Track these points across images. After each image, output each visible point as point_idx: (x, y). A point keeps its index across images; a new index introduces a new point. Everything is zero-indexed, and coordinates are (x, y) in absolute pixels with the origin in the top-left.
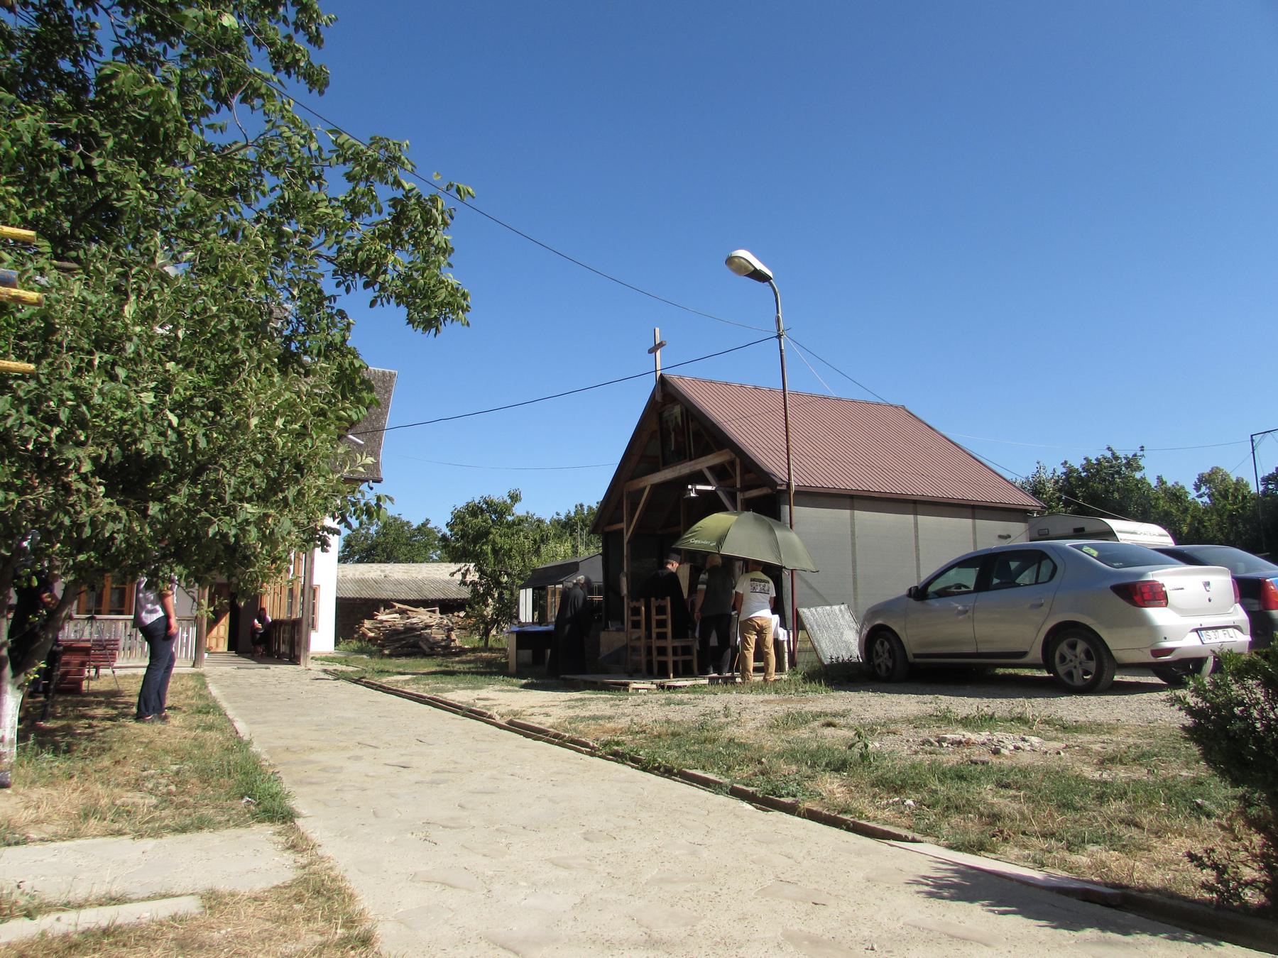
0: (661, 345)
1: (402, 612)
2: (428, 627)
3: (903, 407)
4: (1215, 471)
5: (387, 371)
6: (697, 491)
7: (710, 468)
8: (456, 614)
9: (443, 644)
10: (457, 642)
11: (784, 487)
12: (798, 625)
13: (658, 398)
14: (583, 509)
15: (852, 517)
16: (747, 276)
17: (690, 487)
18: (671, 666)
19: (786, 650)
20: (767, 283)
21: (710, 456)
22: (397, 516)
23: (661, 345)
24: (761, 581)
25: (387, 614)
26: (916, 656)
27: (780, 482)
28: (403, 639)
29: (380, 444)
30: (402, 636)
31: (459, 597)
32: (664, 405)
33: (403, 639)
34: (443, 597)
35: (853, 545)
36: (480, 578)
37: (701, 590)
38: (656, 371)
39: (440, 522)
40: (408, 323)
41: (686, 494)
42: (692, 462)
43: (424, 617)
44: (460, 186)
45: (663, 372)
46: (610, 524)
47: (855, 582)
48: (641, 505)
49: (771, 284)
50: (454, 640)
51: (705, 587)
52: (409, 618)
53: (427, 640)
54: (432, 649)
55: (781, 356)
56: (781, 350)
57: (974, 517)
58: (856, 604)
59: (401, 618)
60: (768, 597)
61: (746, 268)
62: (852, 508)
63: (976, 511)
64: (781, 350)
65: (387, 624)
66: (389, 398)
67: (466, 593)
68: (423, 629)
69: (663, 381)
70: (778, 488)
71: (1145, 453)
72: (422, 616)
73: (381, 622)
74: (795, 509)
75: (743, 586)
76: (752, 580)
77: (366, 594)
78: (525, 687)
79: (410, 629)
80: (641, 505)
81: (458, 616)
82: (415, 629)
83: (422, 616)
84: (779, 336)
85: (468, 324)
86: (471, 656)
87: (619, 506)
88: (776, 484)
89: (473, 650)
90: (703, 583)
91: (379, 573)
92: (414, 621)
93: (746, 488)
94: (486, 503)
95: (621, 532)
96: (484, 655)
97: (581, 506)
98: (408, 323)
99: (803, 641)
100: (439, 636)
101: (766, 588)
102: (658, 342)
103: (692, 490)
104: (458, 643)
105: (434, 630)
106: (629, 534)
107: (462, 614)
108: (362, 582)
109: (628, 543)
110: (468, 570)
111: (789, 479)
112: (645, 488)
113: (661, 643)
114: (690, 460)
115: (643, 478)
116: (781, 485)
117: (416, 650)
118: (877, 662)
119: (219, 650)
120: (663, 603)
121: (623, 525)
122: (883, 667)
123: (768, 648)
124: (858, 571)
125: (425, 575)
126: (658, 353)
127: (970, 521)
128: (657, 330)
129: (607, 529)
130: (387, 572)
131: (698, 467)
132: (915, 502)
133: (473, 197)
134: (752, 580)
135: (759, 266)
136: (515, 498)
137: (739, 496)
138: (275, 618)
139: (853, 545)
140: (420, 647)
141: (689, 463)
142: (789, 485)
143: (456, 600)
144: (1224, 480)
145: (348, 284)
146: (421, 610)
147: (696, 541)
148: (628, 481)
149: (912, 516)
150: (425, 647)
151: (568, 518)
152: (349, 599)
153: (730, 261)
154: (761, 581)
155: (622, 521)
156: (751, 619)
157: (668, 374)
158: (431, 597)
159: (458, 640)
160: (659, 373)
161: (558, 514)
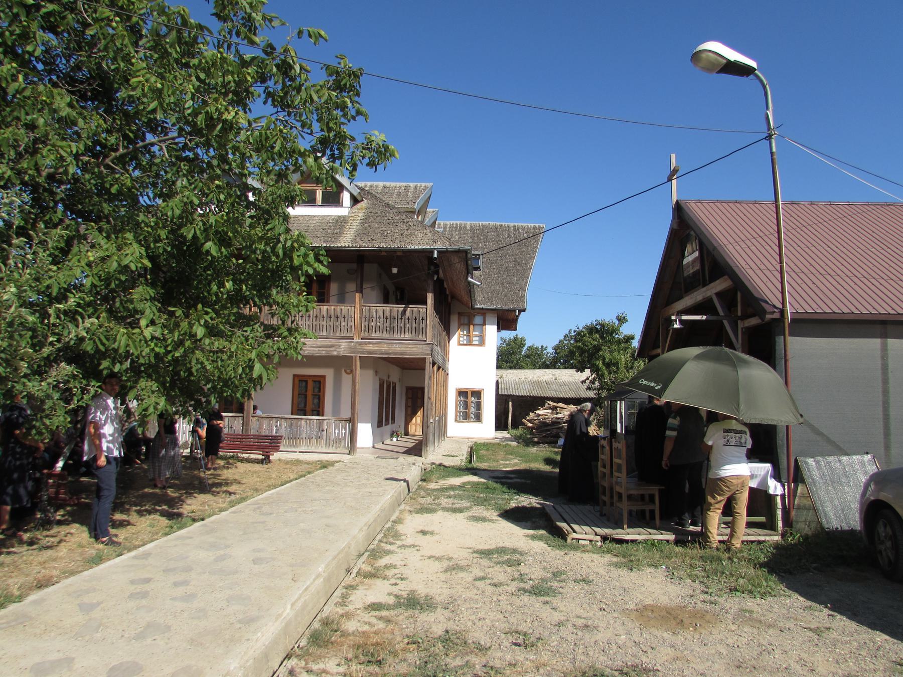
1: (554, 408)
5: (541, 225)
11: (777, 316)
12: (797, 477)
15: (884, 349)
16: (719, 72)
19: (779, 505)
20: (752, 77)
21: (718, 282)
24: (736, 432)
28: (549, 430)
29: (526, 282)
30: (549, 428)
33: (549, 430)
35: (885, 381)
37: (670, 437)
42: (705, 289)
44: (309, 29)
51: (674, 433)
52: (557, 413)
55: (773, 160)
60: (745, 449)
62: (884, 336)
64: (772, 154)
65: (540, 418)
73: (539, 415)
74: (790, 339)
75: (713, 437)
76: (727, 431)
77: (535, 393)
82: (559, 423)
84: (769, 137)
88: (765, 312)
90: (672, 429)
91: (551, 376)
92: (559, 416)
103: (676, 320)
108: (538, 383)
111: (783, 303)
114: (704, 286)
119: (417, 434)
124: (892, 412)
130: (557, 376)
131: (709, 294)
133: (326, 40)
135: (733, 56)
139: (885, 381)
142: (782, 312)
152: (522, 396)
153: (696, 57)
154: (736, 432)
155: (659, 347)
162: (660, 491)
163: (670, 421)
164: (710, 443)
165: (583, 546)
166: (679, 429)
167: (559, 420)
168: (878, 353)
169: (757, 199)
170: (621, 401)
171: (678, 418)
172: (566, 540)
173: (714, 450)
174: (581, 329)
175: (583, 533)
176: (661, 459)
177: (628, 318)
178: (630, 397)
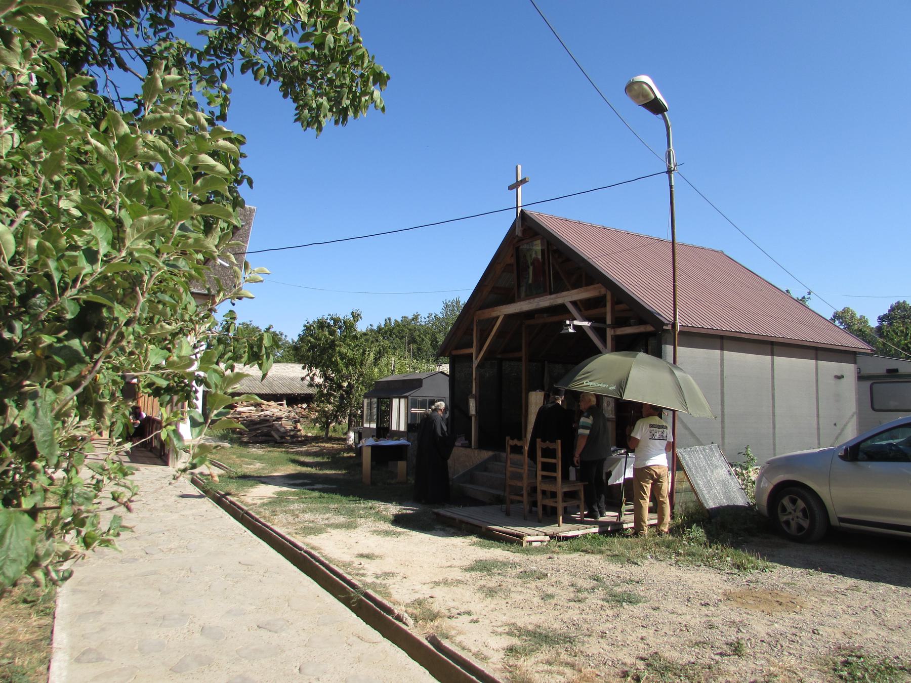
0: (524, 181)
1: (257, 405)
2: (279, 419)
3: (722, 252)
4: (846, 310)
5: (252, 207)
6: (575, 327)
7: (574, 303)
8: (300, 405)
9: (292, 433)
10: (302, 432)
11: (669, 327)
13: (519, 232)
14: (390, 322)
17: (568, 322)
18: (560, 511)
20: (660, 116)
22: (249, 323)
23: (524, 181)
25: (245, 406)
26: (842, 520)
27: (666, 322)
28: (258, 429)
30: (258, 426)
31: (302, 392)
32: (521, 240)
33: (258, 429)
34: (289, 392)
36: (325, 381)
37: (583, 435)
38: (517, 207)
39: (292, 333)
40: (296, 121)
41: (562, 329)
42: (553, 296)
43: (275, 410)
45: (523, 208)
46: (456, 348)
47: (723, 422)
48: (493, 333)
49: (665, 118)
50: (300, 430)
51: (587, 432)
52: (262, 411)
53: (278, 430)
54: (282, 437)
55: (671, 192)
56: (671, 187)
57: (817, 359)
58: (723, 444)
59: (257, 410)
60: (665, 442)
61: (646, 95)
63: (725, 342)
64: (671, 187)
65: (244, 415)
66: (249, 229)
67: (313, 391)
68: (274, 421)
69: (523, 217)
70: (664, 327)
71: (812, 296)
72: (273, 409)
73: (240, 413)
76: (652, 426)
78: (399, 521)
79: (265, 421)
80: (493, 333)
81: (301, 408)
82: (268, 421)
83: (273, 409)
84: (669, 172)
85: (383, 109)
86: (314, 447)
87: (469, 332)
88: (664, 324)
89: (316, 439)
90: (585, 427)
93: (619, 322)
94: (332, 318)
95: (471, 355)
96: (327, 445)
97: (389, 319)
98: (296, 121)
99: (680, 481)
100: (289, 426)
101: (665, 435)
102: (519, 179)
103: (570, 325)
104: (303, 433)
105: (284, 422)
106: (479, 359)
107: (305, 406)
109: (477, 367)
110: (314, 374)
112: (498, 318)
113: (548, 487)
114: (551, 294)
115: (495, 308)
116: (667, 325)
117: (270, 438)
118: (784, 518)
120: (552, 446)
121: (473, 350)
122: (793, 524)
123: (663, 497)
125: (274, 373)
126: (520, 190)
127: (813, 362)
128: (519, 167)
129: (454, 353)
132: (722, 337)
134: (652, 426)
136: (356, 316)
137: (610, 333)
138: (149, 415)
140: (272, 436)
141: (549, 297)
142: (674, 325)
143: (299, 395)
144: (852, 317)
145: (224, 69)
146: (272, 403)
147: (591, 384)
148: (480, 309)
149: (719, 352)
150: (276, 436)
151: (380, 329)
156: (648, 468)
157: (529, 210)
158: (280, 392)
159: (304, 430)
160: (519, 209)
161: (371, 326)
162: (585, 486)
163: (583, 420)
164: (638, 437)
165: (536, 548)
166: (592, 428)
167: (268, 418)
168: (719, 357)
169: (568, 218)
170: (400, 398)
171: (591, 417)
172: (521, 544)
173: (641, 444)
174: (311, 322)
175: (535, 535)
176: (573, 456)
177: (362, 315)
178: (413, 395)
